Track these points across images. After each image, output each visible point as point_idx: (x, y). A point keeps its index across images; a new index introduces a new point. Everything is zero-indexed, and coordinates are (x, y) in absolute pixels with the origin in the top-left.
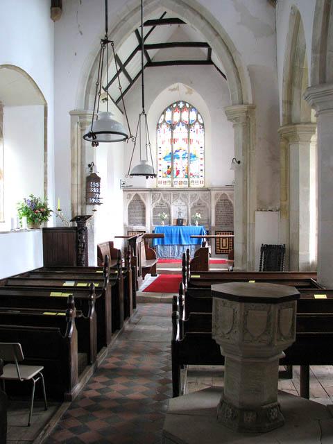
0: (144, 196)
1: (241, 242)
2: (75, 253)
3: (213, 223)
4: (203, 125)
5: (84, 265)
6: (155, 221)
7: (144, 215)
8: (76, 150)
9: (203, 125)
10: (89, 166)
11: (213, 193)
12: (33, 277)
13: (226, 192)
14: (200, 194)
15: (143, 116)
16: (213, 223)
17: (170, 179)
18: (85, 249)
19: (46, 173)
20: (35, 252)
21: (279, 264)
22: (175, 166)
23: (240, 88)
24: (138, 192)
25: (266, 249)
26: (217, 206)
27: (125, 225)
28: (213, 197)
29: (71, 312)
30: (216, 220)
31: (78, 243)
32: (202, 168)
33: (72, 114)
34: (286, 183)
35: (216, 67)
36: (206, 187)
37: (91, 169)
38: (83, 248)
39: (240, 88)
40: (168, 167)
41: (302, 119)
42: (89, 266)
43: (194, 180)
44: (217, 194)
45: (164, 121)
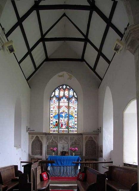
6: (48, 153)
11: (84, 136)
14: (76, 137)
16: (84, 155)
24: (38, 135)
27: (29, 155)
44: (86, 137)
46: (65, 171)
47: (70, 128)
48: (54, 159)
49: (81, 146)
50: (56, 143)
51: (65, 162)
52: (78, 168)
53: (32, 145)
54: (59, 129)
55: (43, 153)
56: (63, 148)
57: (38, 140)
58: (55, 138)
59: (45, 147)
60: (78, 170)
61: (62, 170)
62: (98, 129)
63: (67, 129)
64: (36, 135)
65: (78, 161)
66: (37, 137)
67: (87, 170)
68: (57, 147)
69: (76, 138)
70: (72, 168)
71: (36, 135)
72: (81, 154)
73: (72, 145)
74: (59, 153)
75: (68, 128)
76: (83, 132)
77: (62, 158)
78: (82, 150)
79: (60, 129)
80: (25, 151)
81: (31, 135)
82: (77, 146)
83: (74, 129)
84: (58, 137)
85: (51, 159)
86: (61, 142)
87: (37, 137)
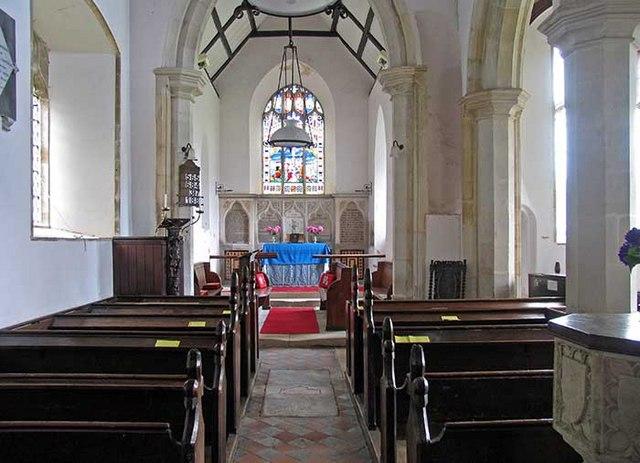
0: (247, 204)
1: (405, 258)
2: (165, 276)
3: (338, 240)
4: (323, 115)
5: (178, 294)
6: (261, 238)
7: (247, 230)
8: (164, 125)
9: (323, 115)
10: (184, 149)
11: (337, 201)
12: (96, 312)
13: (355, 200)
14: (321, 203)
15: (289, 50)
16: (338, 240)
17: (280, 184)
18: (179, 269)
19: (118, 156)
20: (101, 276)
21: (459, 288)
22: (286, 166)
23: (404, 44)
24: (240, 200)
25: (437, 267)
26: (343, 219)
27: (221, 242)
28: (337, 208)
29: (196, 386)
30: (342, 236)
31: (169, 259)
32: (321, 169)
33: (158, 73)
34: (472, 175)
35: (342, 40)
36: (328, 192)
37: (187, 154)
38: (177, 267)
39: (404, 44)
40: (277, 168)
41: (499, 83)
42: (185, 294)
43: (311, 185)
44: (342, 203)
45: (273, 109)
50: (277, 215)
74: (285, 237)
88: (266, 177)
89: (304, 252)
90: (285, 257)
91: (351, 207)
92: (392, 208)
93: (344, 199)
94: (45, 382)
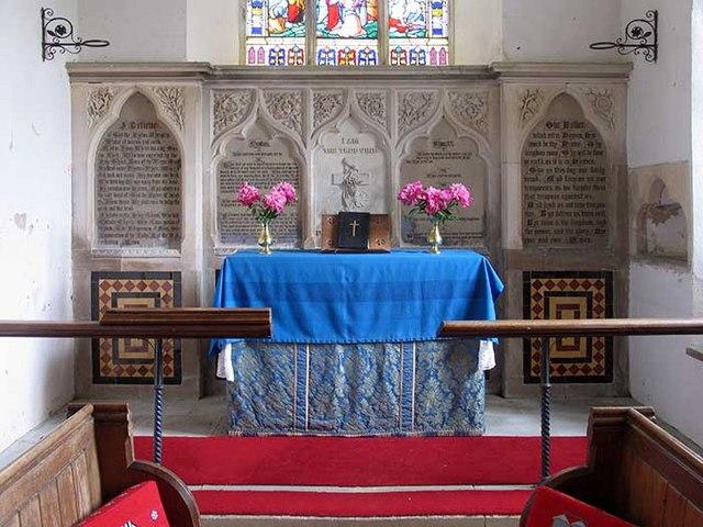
6: (228, 226)
7: (174, 196)
11: (512, 91)
14: (445, 98)
16: (512, 237)
24: (148, 87)
27: (78, 243)
28: (511, 116)
30: (528, 223)
44: (528, 99)
46: (367, 386)
47: (393, 29)
48: (269, 280)
49: (485, 167)
50: (287, 141)
51: (365, 310)
52: (476, 358)
53: (102, 166)
54: (311, 37)
55: (187, 230)
56: (348, 186)
57: (153, 126)
58: (277, 103)
59: (206, 176)
60: (480, 374)
61: (341, 381)
62: (636, 32)
63: (373, 44)
64: (127, 88)
65: (475, 308)
66: (139, 98)
67: (646, 467)
68: (298, 175)
69: (446, 101)
70: (422, 364)
71: (127, 88)
72: (488, 233)
73: (419, 157)
74: (315, 223)
75: (379, 36)
76: (501, 59)
77: (338, 277)
78: (492, 207)
79: (322, 44)
80: (20, 219)
81: (88, 88)
82: (454, 166)
83: (422, 41)
84: (303, 94)
85: (246, 281)
86: (324, 137)
87: (139, 98)
88: (256, 18)
89: (398, 292)
90: (315, 315)
91: (561, 115)
92: (11, 325)
93: (533, 84)
94: (245, 317)
